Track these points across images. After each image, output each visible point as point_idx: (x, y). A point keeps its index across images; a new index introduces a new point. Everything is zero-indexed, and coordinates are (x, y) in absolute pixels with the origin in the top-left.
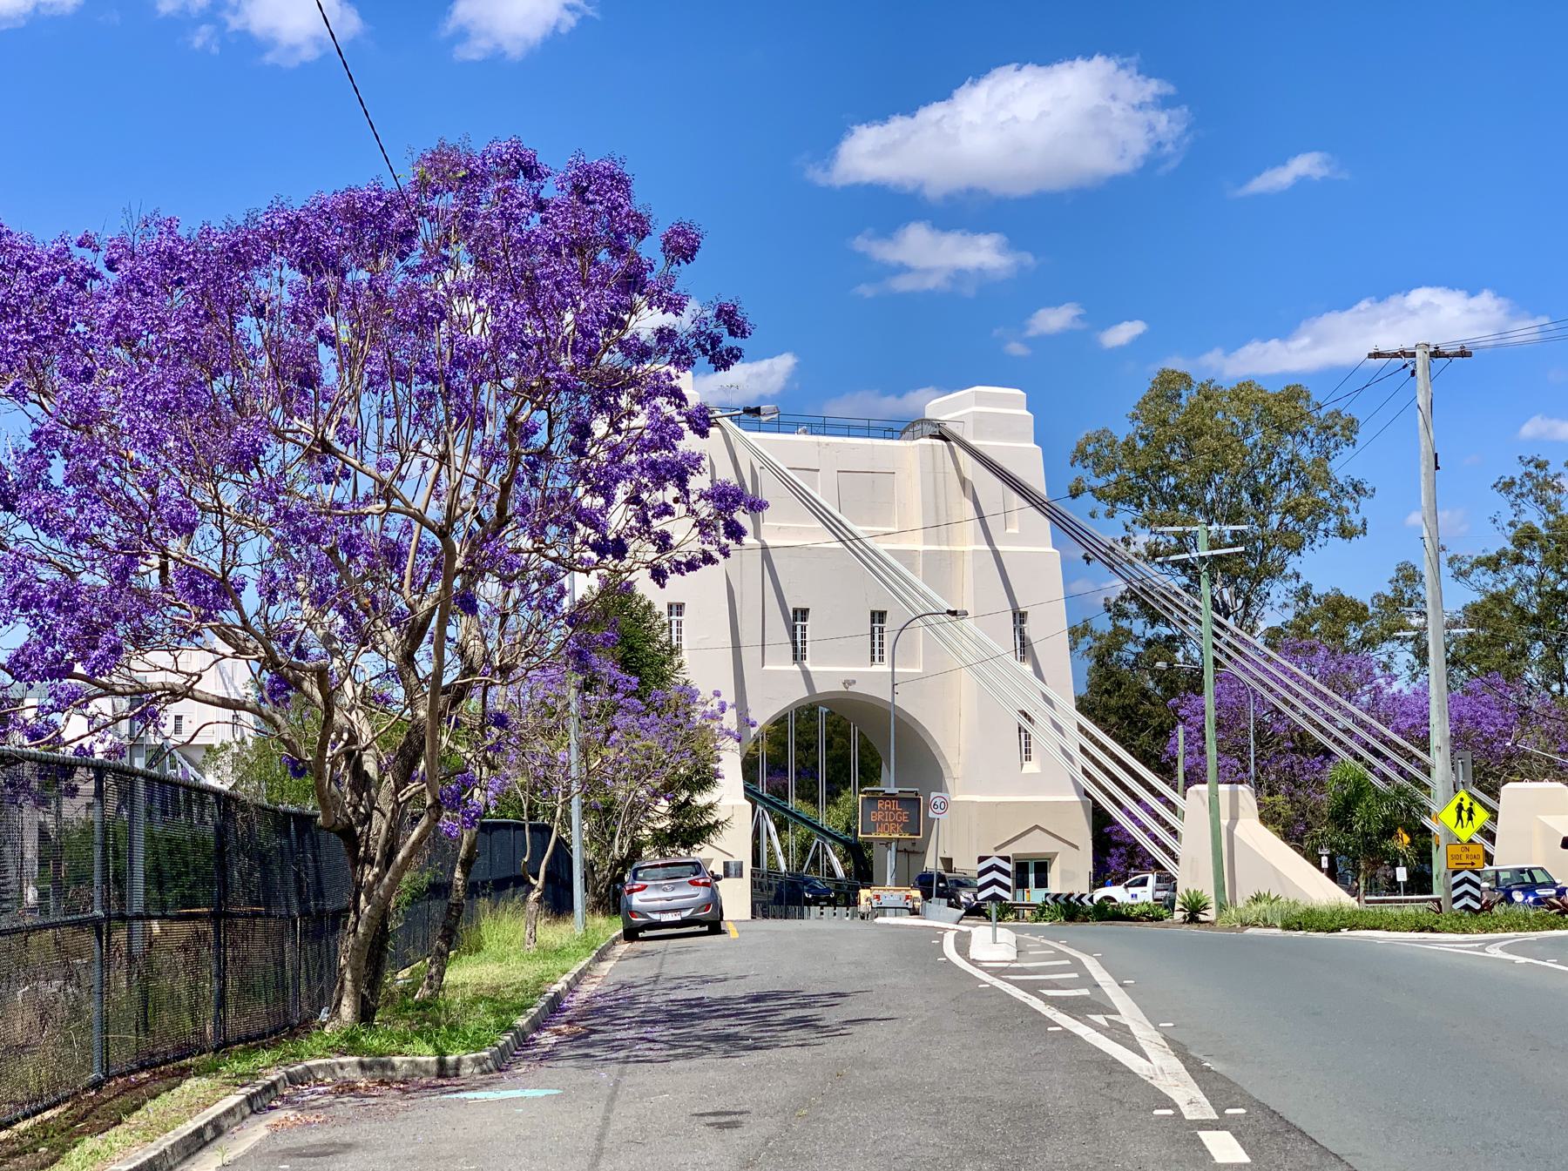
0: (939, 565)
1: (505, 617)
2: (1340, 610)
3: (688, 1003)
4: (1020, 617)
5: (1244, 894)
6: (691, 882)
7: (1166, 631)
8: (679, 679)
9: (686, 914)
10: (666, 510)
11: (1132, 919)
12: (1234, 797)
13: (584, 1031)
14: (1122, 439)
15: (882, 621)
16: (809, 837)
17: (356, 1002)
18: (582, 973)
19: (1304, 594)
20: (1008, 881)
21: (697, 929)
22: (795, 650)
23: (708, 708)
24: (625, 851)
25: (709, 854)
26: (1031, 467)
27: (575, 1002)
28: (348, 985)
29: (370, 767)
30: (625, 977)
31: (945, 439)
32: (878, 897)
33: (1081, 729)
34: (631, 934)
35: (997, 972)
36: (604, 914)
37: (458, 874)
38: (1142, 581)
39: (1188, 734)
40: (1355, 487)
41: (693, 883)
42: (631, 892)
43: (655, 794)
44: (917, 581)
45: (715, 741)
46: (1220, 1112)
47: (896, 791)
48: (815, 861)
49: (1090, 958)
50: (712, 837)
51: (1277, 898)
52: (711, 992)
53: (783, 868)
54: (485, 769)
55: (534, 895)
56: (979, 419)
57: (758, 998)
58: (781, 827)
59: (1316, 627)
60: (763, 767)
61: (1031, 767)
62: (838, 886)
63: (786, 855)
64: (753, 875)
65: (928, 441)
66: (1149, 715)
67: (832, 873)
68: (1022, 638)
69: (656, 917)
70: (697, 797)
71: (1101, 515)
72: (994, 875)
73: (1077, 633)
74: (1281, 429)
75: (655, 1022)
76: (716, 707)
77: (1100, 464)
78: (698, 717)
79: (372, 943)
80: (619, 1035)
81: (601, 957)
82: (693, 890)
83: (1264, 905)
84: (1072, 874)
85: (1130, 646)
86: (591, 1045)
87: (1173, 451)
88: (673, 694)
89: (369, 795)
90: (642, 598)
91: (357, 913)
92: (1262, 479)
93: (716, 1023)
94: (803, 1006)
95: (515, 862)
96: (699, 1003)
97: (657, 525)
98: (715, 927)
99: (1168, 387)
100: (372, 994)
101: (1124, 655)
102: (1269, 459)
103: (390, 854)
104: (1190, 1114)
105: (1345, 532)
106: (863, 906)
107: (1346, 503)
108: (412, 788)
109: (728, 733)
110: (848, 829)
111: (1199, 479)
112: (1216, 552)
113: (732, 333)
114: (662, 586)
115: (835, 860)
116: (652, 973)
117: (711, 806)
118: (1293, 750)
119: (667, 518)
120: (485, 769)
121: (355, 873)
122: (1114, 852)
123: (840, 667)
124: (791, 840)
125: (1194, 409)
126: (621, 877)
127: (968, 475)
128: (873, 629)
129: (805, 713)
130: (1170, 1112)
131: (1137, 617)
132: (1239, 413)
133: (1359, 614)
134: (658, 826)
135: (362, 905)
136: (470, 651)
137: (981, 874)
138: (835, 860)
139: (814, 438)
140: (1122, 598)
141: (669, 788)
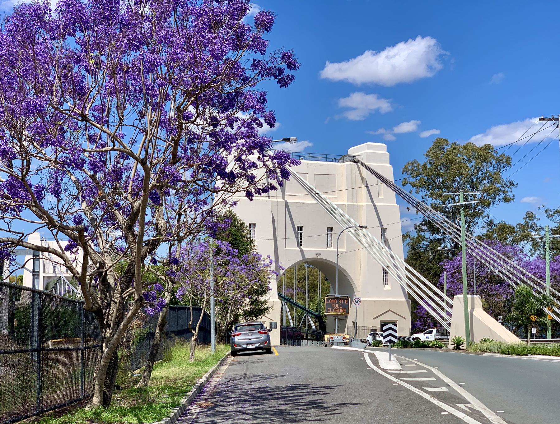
0: (353, 210)
1: (180, 215)
2: (505, 229)
3: (260, 390)
4: (384, 230)
5: (477, 339)
6: (259, 332)
7: (437, 237)
8: (254, 252)
9: (257, 345)
10: (254, 165)
11: (430, 347)
12: (473, 299)
13: (213, 405)
14: (422, 164)
15: (331, 231)
16: (302, 313)
17: (100, 396)
18: (213, 372)
19: (491, 223)
21: (261, 351)
22: (298, 242)
23: (266, 262)
24: (232, 318)
25: (265, 320)
26: (388, 173)
27: (209, 388)
28: (97, 387)
29: (111, 280)
30: (231, 374)
31: (356, 162)
32: (332, 338)
33: (406, 269)
34: (234, 353)
36: (223, 344)
37: (157, 331)
38: (429, 217)
39: (447, 275)
40: (510, 183)
41: (260, 333)
42: (234, 336)
43: (244, 296)
44: (345, 214)
45: (268, 275)
47: (339, 296)
48: (304, 323)
49: (416, 361)
50: (266, 313)
51: (492, 340)
52: (270, 384)
53: (292, 326)
54: (170, 283)
55: (194, 338)
56: (369, 155)
57: (292, 388)
58: (291, 309)
59: (495, 235)
60: (284, 287)
61: (387, 287)
62: (313, 332)
63: (293, 321)
64: (281, 327)
65: (349, 163)
66: (431, 268)
67: (311, 327)
68: (384, 238)
69: (245, 346)
70: (260, 298)
71: (414, 192)
72: (390, 332)
73: (405, 237)
74: (483, 161)
75: (246, 401)
76: (269, 262)
77: (414, 174)
78: (261, 266)
79: (109, 367)
80: (229, 408)
81: (222, 364)
82: (260, 335)
83: (488, 343)
84: (404, 329)
85: (424, 242)
86: (215, 415)
87: (441, 169)
88: (251, 257)
89: (110, 294)
90: (240, 220)
91: (102, 351)
92: (475, 180)
93: (274, 403)
94: (314, 394)
95: (184, 323)
96: (264, 390)
97: (250, 172)
98: (268, 351)
99: (439, 144)
100: (109, 391)
101: (422, 245)
102: (478, 171)
103: (117, 324)
105: (506, 200)
106: (326, 341)
107: (507, 189)
108: (130, 290)
109: (273, 272)
110: (317, 310)
111: (448, 180)
112: (467, 203)
113: (289, 67)
114: (251, 200)
115: (312, 323)
116: (243, 373)
117: (266, 301)
118: (488, 282)
119: (254, 168)
120: (170, 283)
121: (102, 332)
122: (421, 320)
123: (314, 248)
124: (295, 314)
125: (449, 153)
126: (231, 329)
127: (364, 176)
128: (327, 235)
129: (300, 266)
131: (427, 231)
132: (467, 155)
133: (512, 231)
134: (245, 309)
135: (104, 349)
136: (160, 226)
138: (312, 323)
140: (421, 224)
141: (250, 294)
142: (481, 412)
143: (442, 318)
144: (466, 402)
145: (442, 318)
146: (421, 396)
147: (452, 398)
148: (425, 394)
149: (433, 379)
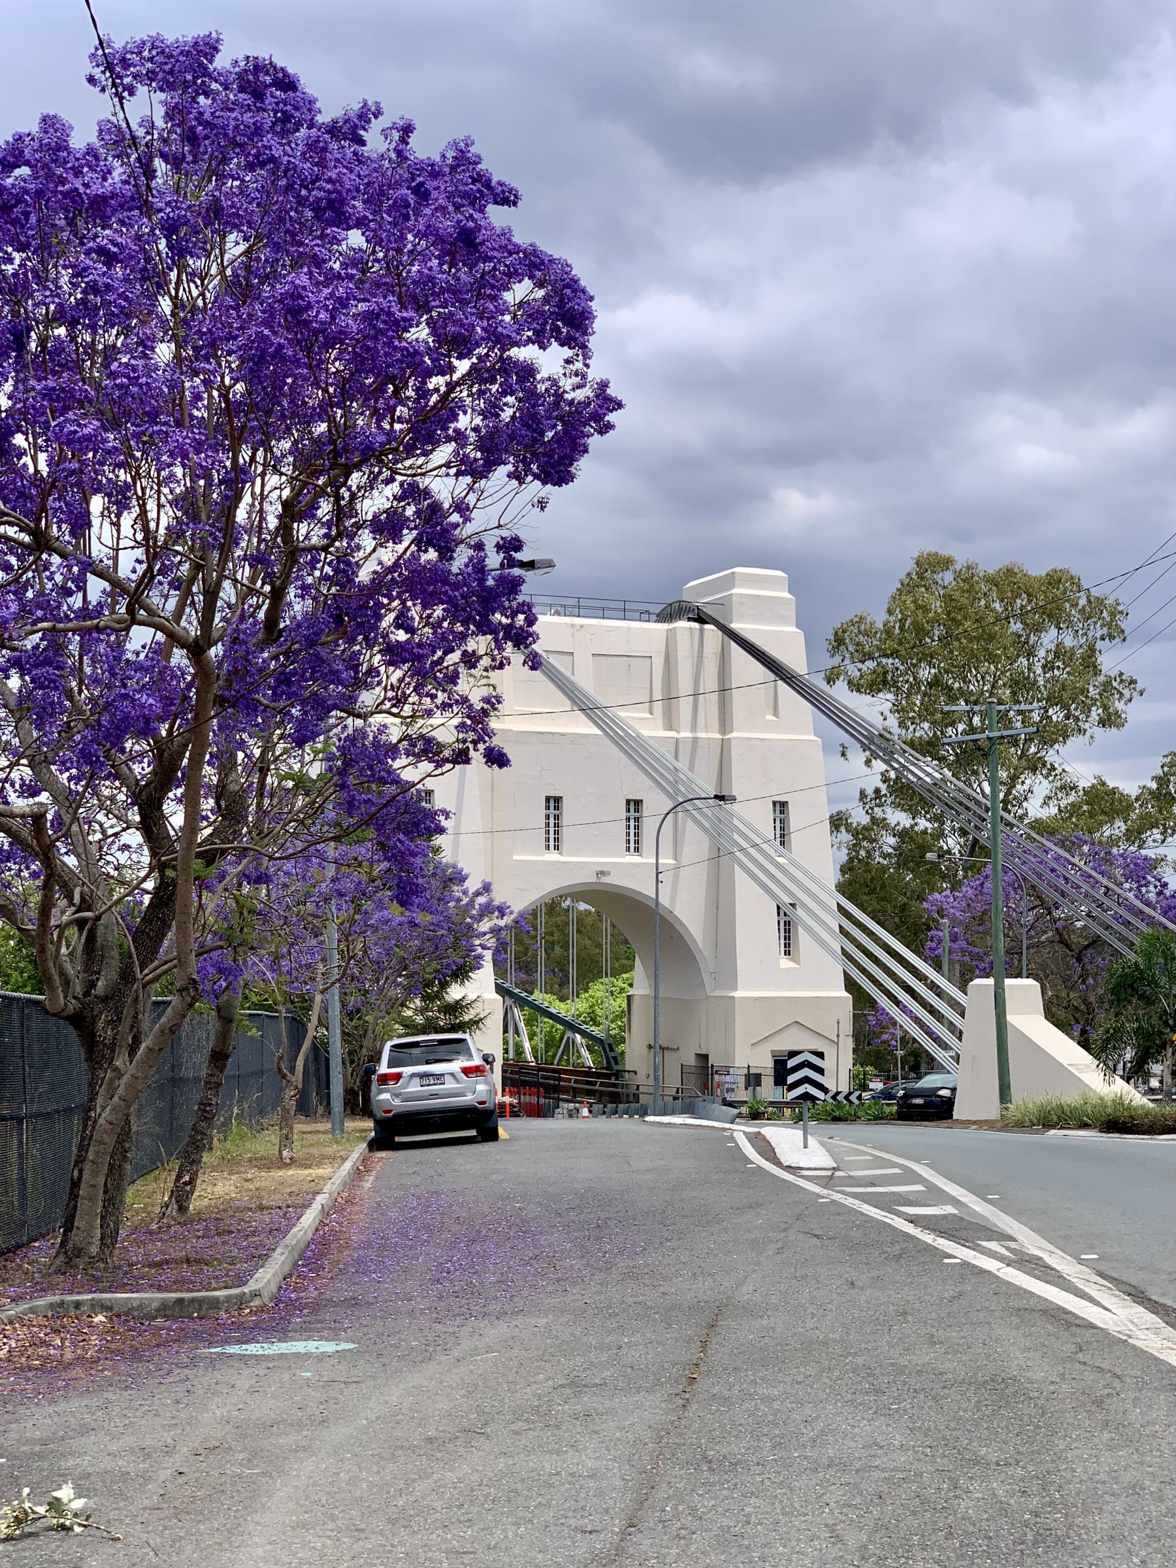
35: (828, 1182)
72: (806, 1072)
73: (838, 822)
84: (838, 1072)
122: (875, 1044)
123: (595, 856)
139: (568, 620)
142: (1040, 1259)
143: (937, 1039)
145: (937, 1039)
146: (890, 1226)
147: (964, 1229)
148: (901, 1220)
149: (919, 1188)
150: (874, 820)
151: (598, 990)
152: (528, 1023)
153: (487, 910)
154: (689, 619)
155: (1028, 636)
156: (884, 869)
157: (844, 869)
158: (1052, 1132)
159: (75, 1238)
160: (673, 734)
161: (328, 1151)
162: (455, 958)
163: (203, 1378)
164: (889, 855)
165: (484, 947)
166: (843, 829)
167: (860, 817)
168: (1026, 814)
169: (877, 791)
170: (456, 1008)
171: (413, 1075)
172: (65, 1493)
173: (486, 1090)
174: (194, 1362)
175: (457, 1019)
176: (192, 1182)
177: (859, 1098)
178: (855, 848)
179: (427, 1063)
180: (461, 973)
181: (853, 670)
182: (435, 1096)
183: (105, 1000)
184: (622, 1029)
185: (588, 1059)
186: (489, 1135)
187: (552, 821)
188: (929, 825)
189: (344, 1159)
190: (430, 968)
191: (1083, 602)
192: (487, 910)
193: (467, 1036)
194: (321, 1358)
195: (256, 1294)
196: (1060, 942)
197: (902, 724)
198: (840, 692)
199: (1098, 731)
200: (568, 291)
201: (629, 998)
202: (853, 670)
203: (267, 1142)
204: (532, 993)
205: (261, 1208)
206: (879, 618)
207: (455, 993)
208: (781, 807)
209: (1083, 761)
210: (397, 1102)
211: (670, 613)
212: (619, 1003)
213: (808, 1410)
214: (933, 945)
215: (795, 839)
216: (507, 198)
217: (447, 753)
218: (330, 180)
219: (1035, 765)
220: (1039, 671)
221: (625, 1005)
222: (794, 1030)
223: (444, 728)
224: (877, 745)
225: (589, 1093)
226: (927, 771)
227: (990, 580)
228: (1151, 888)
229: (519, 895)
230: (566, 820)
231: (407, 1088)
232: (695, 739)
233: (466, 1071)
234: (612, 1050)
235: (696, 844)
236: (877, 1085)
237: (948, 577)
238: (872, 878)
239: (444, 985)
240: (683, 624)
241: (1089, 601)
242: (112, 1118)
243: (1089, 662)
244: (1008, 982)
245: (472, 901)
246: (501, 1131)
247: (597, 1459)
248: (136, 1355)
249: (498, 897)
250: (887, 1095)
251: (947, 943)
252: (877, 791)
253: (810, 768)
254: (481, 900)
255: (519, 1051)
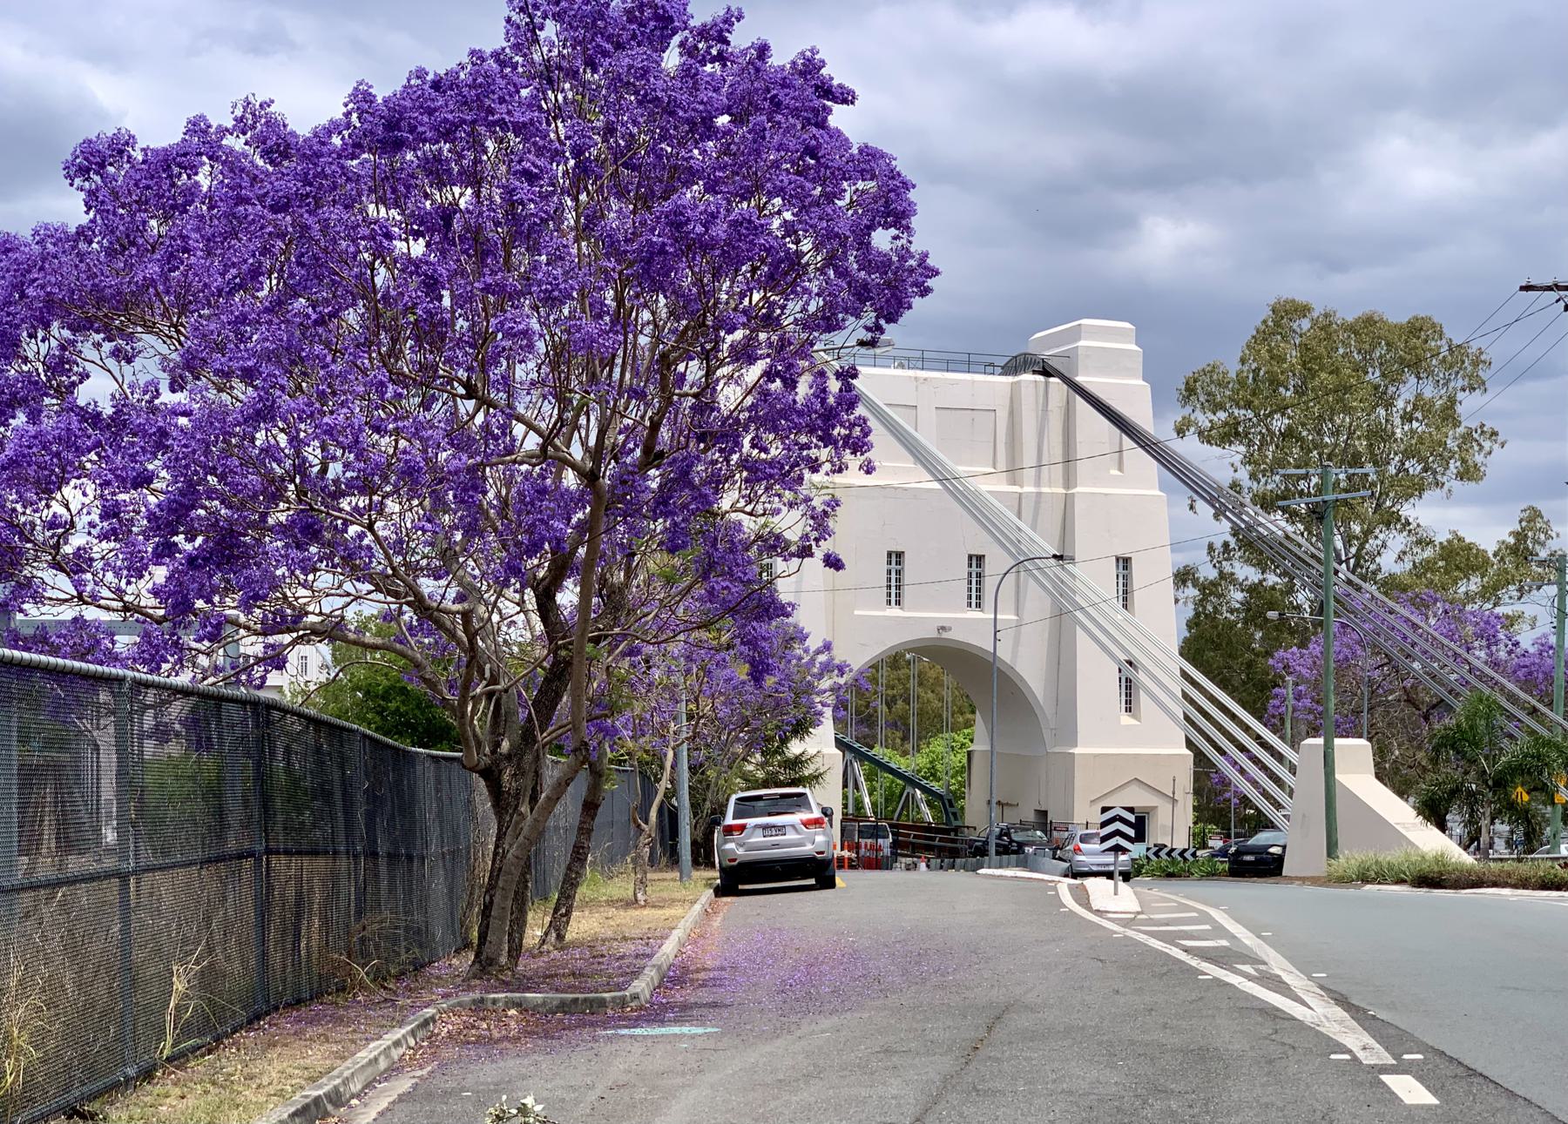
20: (1131, 832)
33: (1184, 674)
35: (1126, 923)
46: (1397, 1057)
84: (1175, 826)
104: (1367, 1059)
122: (1216, 804)
123: (941, 612)
128: (970, 574)
130: (1347, 1057)
137: (1104, 825)
139: (911, 373)
144: (1255, 961)
150: (1222, 575)
151: (938, 745)
152: (868, 779)
153: (827, 668)
154: (1035, 372)
155: (1386, 387)
156: (1232, 625)
157: (1191, 624)
158: (1368, 887)
159: (488, 950)
160: (1016, 489)
161: (677, 895)
162: (793, 714)
163: (606, 1050)
164: (1237, 610)
165: (824, 705)
166: (1189, 584)
167: (1208, 573)
168: (1379, 570)
169: (1226, 545)
170: (798, 762)
171: (757, 826)
172: (529, 1101)
173: (823, 842)
174: (595, 1039)
175: (797, 772)
176: (568, 914)
177: (1194, 855)
178: (1201, 603)
179: (770, 814)
180: (801, 728)
181: (1203, 419)
182: (776, 846)
183: (509, 757)
184: (962, 785)
185: (928, 815)
186: (828, 883)
187: (893, 576)
188: (1278, 580)
189: (693, 902)
190: (770, 724)
191: (1444, 350)
192: (827, 668)
193: (807, 791)
194: (693, 1037)
195: (635, 997)
196: (1408, 701)
197: (1253, 476)
198: (1190, 449)
199: (1456, 485)
200: (892, 195)
201: (969, 753)
202: (1203, 419)
203: (622, 887)
204: (872, 747)
205: (625, 939)
206: (1232, 368)
207: (795, 748)
208: (1125, 563)
209: (1439, 515)
210: (740, 851)
211: (1016, 366)
212: (959, 759)
213: (1056, 1065)
214: (1277, 702)
215: (1138, 597)
216: (846, 97)
217: (793, 549)
218: (702, 103)
219: (1391, 520)
220: (1398, 421)
221: (965, 761)
222: (1134, 788)
223: (791, 524)
224: (1220, 501)
225: (929, 848)
226: (1276, 524)
227: (1352, 329)
228: (1502, 646)
229: (857, 654)
230: (908, 577)
231: (752, 839)
232: (1039, 494)
233: (806, 824)
234: (951, 806)
235: (1037, 603)
236: (1216, 843)
237: (1306, 324)
238: (1219, 635)
239: (784, 741)
240: (1028, 377)
241: (1450, 349)
242: (518, 853)
243: (1448, 414)
244: (1338, 741)
245: (813, 660)
246: (838, 880)
247: (901, 1090)
248: (547, 1035)
249: (839, 656)
250: (1223, 852)
251: (1291, 701)
252: (1226, 545)
253: (1140, 533)
254: (822, 658)
255: (859, 804)
